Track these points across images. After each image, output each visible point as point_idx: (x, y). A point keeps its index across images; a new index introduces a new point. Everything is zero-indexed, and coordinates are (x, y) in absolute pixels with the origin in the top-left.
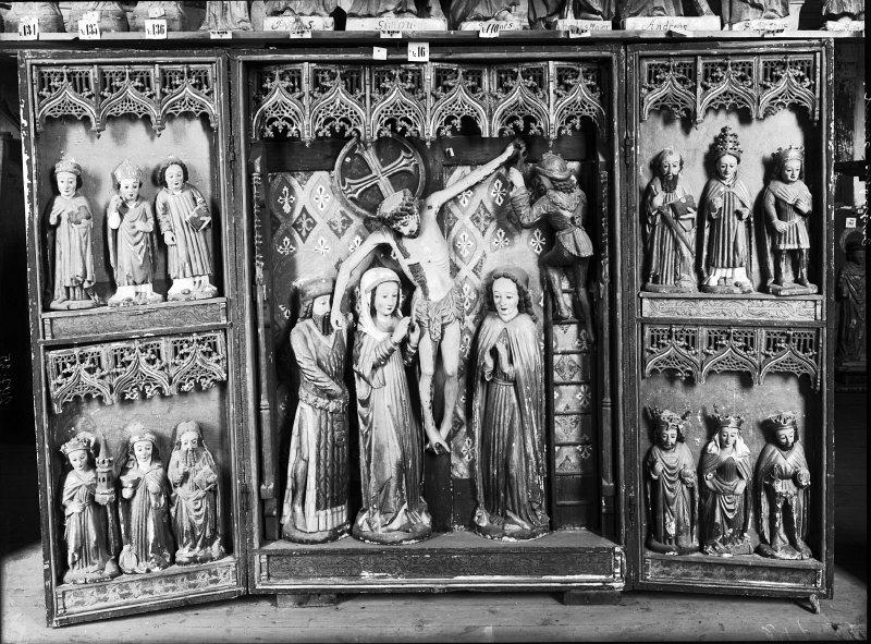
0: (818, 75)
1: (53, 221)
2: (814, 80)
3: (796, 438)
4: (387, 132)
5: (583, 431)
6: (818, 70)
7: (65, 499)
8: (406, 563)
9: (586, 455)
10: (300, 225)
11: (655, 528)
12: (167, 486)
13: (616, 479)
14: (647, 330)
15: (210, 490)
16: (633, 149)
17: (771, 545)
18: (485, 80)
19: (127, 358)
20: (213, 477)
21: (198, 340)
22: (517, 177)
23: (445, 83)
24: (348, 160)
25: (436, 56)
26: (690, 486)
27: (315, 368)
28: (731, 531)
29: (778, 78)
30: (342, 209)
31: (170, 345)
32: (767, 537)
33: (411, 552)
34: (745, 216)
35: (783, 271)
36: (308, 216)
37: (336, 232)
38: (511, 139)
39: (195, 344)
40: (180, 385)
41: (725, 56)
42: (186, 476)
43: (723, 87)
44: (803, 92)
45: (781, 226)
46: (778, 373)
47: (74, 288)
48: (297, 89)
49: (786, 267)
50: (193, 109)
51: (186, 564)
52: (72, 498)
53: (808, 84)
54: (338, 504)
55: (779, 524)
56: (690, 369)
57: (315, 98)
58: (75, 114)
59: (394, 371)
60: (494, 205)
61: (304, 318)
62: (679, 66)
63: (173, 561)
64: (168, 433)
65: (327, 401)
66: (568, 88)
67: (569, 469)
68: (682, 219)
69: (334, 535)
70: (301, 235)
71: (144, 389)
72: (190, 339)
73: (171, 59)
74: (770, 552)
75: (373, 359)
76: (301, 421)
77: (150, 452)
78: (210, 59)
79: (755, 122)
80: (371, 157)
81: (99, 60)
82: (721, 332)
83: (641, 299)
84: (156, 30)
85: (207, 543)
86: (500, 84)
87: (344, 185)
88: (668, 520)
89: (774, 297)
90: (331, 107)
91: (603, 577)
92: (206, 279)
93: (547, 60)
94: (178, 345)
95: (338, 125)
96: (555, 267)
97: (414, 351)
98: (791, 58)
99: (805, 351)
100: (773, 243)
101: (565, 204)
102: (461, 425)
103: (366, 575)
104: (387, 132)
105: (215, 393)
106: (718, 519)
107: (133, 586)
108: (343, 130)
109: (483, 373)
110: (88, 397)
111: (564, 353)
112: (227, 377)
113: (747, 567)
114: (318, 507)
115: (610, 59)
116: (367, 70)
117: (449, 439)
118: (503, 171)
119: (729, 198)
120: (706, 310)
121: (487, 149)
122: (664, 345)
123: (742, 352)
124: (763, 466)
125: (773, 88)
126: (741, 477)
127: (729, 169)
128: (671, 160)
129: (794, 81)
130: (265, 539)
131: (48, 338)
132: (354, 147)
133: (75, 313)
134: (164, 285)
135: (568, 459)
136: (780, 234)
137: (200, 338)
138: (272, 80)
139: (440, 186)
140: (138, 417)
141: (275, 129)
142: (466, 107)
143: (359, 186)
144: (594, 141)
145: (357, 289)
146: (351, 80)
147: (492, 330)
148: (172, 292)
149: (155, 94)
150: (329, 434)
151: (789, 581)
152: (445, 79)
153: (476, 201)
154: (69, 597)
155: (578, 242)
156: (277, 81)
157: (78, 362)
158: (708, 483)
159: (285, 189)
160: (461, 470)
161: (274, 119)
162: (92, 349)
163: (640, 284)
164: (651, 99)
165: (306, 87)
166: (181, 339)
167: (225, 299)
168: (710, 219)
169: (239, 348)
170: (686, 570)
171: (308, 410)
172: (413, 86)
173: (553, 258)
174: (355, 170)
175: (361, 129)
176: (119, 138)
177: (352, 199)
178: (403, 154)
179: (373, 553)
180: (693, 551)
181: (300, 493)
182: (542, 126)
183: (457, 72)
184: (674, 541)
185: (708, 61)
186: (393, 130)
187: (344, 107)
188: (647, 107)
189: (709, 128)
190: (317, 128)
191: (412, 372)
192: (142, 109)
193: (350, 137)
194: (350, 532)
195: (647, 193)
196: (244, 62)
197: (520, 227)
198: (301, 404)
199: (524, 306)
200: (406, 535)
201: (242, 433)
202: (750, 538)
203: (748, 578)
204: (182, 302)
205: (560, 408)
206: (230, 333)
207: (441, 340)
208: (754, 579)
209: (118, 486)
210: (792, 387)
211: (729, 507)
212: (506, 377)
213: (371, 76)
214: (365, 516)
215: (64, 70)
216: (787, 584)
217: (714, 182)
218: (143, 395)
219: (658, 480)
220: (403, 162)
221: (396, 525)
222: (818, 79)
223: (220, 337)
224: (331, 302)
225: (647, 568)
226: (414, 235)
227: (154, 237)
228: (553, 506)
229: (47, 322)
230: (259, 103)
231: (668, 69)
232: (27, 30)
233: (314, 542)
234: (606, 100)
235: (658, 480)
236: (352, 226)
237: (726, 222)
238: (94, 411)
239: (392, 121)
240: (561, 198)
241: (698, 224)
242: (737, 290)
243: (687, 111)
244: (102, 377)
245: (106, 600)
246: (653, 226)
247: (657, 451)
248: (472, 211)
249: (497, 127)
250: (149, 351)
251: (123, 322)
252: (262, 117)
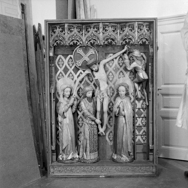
48: (63, 31)
66: (141, 30)
90: (73, 36)
108: (77, 43)
114: (90, 152)
125: (148, 32)
138: (56, 29)
147: (119, 100)
155: (142, 75)
156: (58, 29)
182: (116, 42)
190: (69, 42)
193: (79, 45)
199: (127, 94)
207: (103, 101)
214: (61, 156)
226: (97, 71)
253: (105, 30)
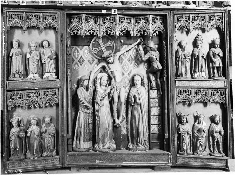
0: (224, 18)
1: (11, 55)
2: (223, 20)
3: (220, 121)
4: (105, 34)
5: (159, 121)
6: (224, 17)
7: (11, 135)
8: (109, 158)
9: (159, 127)
10: (80, 61)
11: (180, 148)
12: (41, 133)
13: (169, 133)
14: (177, 90)
15: (53, 135)
16: (173, 39)
17: (213, 152)
18: (132, 20)
19: (30, 95)
20: (54, 132)
21: (50, 91)
22: (141, 47)
24: (94, 43)
25: (119, 13)
26: (190, 135)
27: (84, 100)
28: (202, 148)
29: (213, 20)
30: (92, 57)
31: (43, 92)
32: (212, 150)
33: (110, 154)
34: (204, 57)
35: (215, 73)
36: (82, 58)
37: (90, 63)
38: (140, 37)
39: (50, 92)
40: (45, 104)
41: (198, 14)
42: (46, 131)
43: (197, 22)
44: (219, 23)
45: (214, 60)
46: (214, 102)
47: (16, 74)
49: (216, 71)
50: (52, 26)
51: (45, 157)
52: (13, 135)
53: (221, 21)
54: (89, 141)
55: (215, 146)
56: (190, 101)
57: (85, 24)
58: (19, 26)
59: (106, 101)
60: (134, 56)
61: (81, 86)
62: (185, 17)
63: (42, 156)
64: (41, 118)
65: (87, 110)
67: (155, 132)
68: (187, 59)
69: (88, 150)
70: (80, 64)
71: (35, 105)
72: (49, 90)
73: (46, 12)
74: (213, 154)
75: (100, 98)
76: (79, 116)
77: (36, 123)
78: (56, 12)
79: (206, 32)
80: (100, 41)
81: (26, 11)
82: (198, 91)
83: (176, 81)
84: (42, 3)
85: (52, 151)
86: (136, 22)
87: (93, 50)
88: (184, 145)
89: (213, 80)
90: (90, 27)
91: (166, 162)
92: (54, 74)
94: (45, 92)
95: (92, 32)
96: (151, 73)
97: (112, 96)
98: (216, 14)
99: (222, 95)
100: (212, 65)
101: (154, 54)
102: (124, 119)
103: (97, 161)
104: (105, 34)
105: (55, 108)
106: (198, 145)
107: (29, 163)
108: (93, 33)
109: (131, 103)
110: (19, 106)
111: (153, 98)
112: (59, 102)
113: (207, 159)
114: (84, 141)
115: (167, 14)
116: (100, 17)
117: (121, 122)
118: (136, 47)
119: (199, 53)
120: (194, 84)
121: (132, 40)
122: (182, 94)
123: (204, 96)
124: (210, 129)
125: (211, 22)
126: (204, 132)
127: (200, 44)
128: (183, 42)
129: (217, 20)
130: (68, 151)
131: (7, 88)
132: (96, 39)
133: (16, 81)
134: (42, 75)
135: (155, 129)
136: (214, 62)
137: (51, 90)
138: (73, 19)
139: (119, 50)
140: (33, 113)
141: (74, 33)
142: (127, 28)
143: (96, 51)
144: (163, 37)
145: (96, 79)
146: (96, 20)
147: (134, 91)
148: (44, 77)
149: (41, 21)
150: (88, 120)
151: (219, 163)
152: (121, 19)
153: (129, 55)
154: (10, 165)
155: (157, 65)
156: (75, 19)
157: (16, 95)
158: (195, 135)
159: (76, 51)
160: (124, 132)
161: (74, 30)
162: (20, 92)
163: (175, 78)
164: (178, 26)
165: (84, 21)
166: (46, 90)
167: (58, 79)
168: (195, 59)
169: (62, 94)
170: (189, 160)
171: (82, 113)
172: (113, 21)
173: (151, 70)
174: (96, 45)
175: (98, 33)
176: (29, 33)
177: (95, 54)
178: (109, 41)
179: (100, 155)
180: (191, 154)
181: (79, 137)
182: (148, 33)
183: (125, 18)
184: (185, 151)
185: (193, 15)
186: (107, 34)
187: (93, 27)
188: (177, 28)
189: (194, 33)
190: (86, 32)
191: (111, 102)
192: (37, 25)
194: (93, 150)
195: (177, 52)
196: (66, 13)
197: (142, 61)
198: (80, 111)
199: (142, 84)
200: (109, 150)
201: (63, 118)
202: (208, 151)
203: (207, 162)
204: (46, 80)
205: (152, 114)
206: (60, 89)
207: (119, 93)
208: (209, 162)
209: (26, 133)
210: (218, 106)
211: (201, 141)
212: (138, 104)
213: (101, 19)
215: (16, 13)
216: (218, 164)
217: (195, 49)
218: (35, 107)
219: (181, 134)
220: (109, 43)
221: (106, 147)
222: (224, 20)
223: (57, 90)
224: (89, 82)
225: (178, 160)
227: (40, 61)
228: (151, 142)
229: (8, 83)
230: (69, 25)
231: (182, 17)
232: (5, 2)
233: (83, 152)
234: (165, 27)
235: (181, 134)
236: (95, 61)
237: (199, 59)
238: (19, 110)
239: (107, 31)
240: (153, 52)
241: (191, 61)
242: (203, 78)
243: (188, 29)
244: (23, 100)
245: (21, 166)
246: (179, 61)
247: (180, 125)
248: (128, 58)
249: (135, 33)
250: (37, 93)
251: (30, 85)
252: (71, 30)
253: (120, 22)
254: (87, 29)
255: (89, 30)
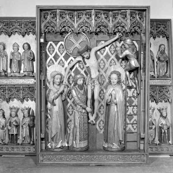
23: (133, 16)
51: (136, 86)
93: (57, 9)
114: (80, 141)
156: (84, 16)
190: (61, 28)
205: (44, 134)
214: (50, 144)
254: (62, 25)
255: (64, 27)
